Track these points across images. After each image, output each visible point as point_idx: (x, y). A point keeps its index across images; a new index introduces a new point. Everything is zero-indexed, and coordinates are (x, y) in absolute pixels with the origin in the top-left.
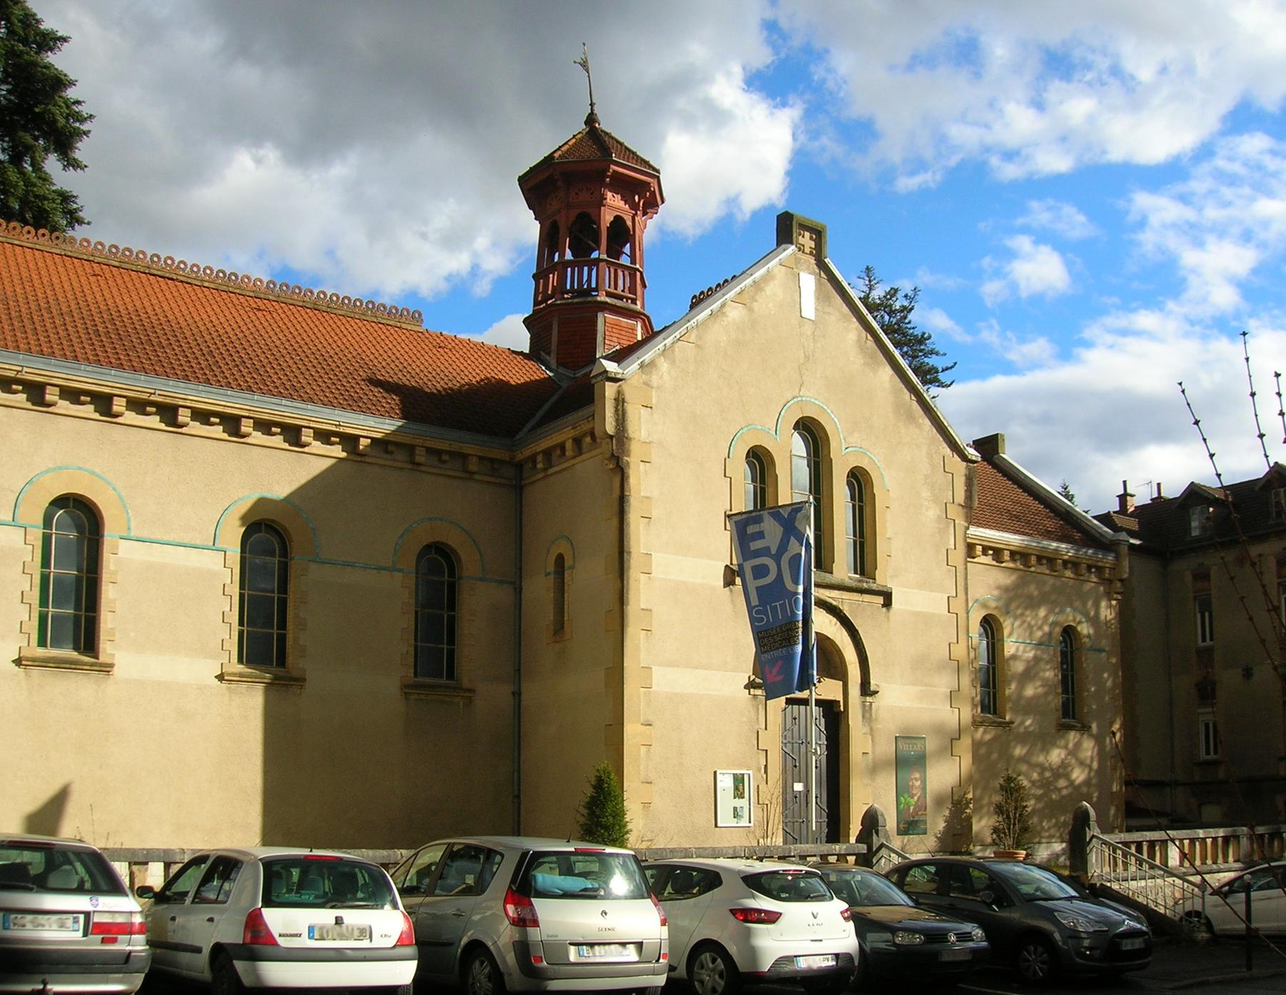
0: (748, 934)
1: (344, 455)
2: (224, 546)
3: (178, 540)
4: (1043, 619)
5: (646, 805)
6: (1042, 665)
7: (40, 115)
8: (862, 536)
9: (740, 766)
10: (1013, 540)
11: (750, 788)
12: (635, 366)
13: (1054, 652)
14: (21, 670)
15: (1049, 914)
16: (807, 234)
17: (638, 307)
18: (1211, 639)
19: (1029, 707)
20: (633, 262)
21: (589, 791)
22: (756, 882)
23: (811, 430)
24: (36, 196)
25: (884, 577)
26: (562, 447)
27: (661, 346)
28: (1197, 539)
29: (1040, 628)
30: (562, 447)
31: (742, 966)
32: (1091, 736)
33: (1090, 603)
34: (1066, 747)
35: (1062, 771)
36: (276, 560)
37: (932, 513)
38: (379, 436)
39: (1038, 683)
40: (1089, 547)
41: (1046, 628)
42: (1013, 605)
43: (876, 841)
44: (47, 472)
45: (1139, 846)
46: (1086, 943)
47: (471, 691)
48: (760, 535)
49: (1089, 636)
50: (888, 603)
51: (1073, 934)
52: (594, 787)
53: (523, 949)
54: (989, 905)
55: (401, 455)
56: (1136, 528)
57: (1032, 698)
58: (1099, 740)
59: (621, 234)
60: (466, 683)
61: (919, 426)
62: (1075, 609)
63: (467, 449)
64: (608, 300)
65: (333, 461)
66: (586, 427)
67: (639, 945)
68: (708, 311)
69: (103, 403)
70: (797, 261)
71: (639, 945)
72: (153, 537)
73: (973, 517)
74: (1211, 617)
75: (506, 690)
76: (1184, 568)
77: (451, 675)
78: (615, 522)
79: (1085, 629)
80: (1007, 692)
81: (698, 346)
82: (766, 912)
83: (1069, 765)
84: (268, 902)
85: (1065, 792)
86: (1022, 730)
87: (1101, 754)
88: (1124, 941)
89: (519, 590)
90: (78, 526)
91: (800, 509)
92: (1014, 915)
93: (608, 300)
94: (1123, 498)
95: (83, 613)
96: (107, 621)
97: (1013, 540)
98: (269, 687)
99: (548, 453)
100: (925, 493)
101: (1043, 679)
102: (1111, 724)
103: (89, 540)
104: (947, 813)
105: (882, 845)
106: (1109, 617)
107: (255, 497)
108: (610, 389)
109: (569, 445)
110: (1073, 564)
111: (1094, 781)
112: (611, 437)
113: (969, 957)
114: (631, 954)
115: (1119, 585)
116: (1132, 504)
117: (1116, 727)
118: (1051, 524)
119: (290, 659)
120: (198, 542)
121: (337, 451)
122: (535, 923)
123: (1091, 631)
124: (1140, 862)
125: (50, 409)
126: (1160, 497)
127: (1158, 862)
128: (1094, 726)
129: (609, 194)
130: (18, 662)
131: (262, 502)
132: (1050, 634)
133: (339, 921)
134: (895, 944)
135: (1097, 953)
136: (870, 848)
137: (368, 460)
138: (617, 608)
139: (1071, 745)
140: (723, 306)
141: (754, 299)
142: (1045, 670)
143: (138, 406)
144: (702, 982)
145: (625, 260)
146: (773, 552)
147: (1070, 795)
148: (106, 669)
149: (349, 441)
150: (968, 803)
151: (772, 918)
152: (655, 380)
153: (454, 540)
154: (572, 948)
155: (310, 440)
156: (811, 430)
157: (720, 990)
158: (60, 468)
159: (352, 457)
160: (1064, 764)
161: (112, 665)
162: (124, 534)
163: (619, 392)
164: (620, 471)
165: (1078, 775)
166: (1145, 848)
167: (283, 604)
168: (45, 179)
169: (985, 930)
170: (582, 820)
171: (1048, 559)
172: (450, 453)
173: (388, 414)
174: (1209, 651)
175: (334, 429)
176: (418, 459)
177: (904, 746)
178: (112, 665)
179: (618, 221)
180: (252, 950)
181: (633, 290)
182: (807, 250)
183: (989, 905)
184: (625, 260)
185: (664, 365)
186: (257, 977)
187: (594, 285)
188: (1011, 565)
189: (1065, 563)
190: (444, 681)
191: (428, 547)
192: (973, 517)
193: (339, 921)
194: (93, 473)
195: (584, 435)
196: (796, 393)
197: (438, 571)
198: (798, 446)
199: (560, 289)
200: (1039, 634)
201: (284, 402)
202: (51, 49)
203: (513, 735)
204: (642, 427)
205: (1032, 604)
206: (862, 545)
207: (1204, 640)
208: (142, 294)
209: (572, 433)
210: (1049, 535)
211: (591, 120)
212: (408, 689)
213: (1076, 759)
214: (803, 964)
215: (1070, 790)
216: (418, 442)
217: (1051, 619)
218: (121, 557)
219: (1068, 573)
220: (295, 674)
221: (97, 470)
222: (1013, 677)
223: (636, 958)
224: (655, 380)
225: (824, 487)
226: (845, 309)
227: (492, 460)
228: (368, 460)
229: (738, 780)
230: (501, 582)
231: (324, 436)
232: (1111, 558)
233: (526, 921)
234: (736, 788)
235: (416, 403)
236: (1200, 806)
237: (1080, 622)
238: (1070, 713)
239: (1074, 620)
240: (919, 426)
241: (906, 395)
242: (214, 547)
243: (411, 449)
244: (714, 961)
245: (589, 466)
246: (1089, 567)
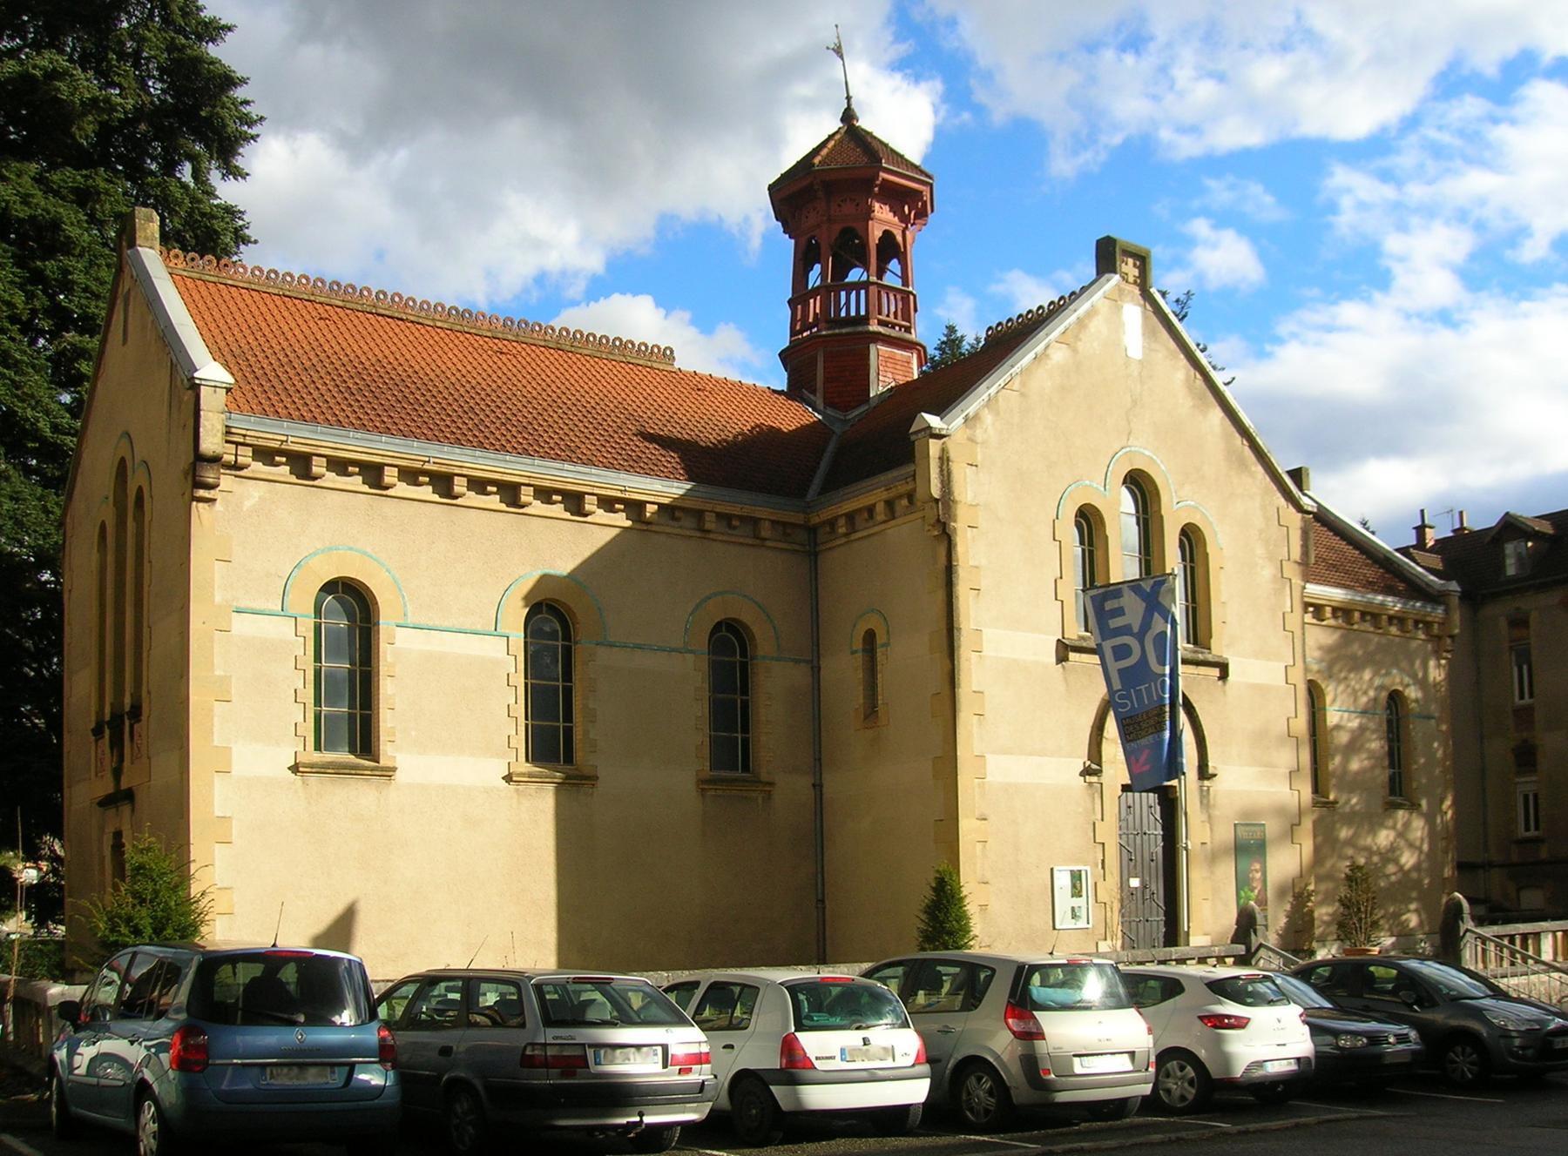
0: (1219, 1040)
1: (628, 523)
2: (507, 632)
3: (457, 626)
4: (1368, 683)
5: (984, 907)
6: (1368, 733)
7: (208, 121)
8: (1194, 601)
9: (1077, 862)
10: (1336, 594)
11: (1087, 885)
12: (960, 420)
13: (1377, 723)
14: (298, 778)
15: (1478, 1013)
16: (1130, 261)
17: (912, 337)
18: (1531, 696)
19: (1352, 783)
20: (905, 282)
21: (930, 894)
22: (1221, 988)
23: (1140, 485)
24: (203, 215)
25: (1220, 647)
26: (870, 510)
27: (985, 397)
28: (1513, 580)
29: (1365, 693)
30: (870, 510)
31: (1215, 1072)
32: (1421, 814)
33: (1418, 663)
34: (1394, 828)
35: (1390, 855)
36: (560, 643)
37: (1267, 572)
38: (666, 501)
39: (1364, 756)
40: (1417, 599)
41: (1372, 693)
42: (1336, 669)
43: (1255, 941)
44: (315, 554)
45: (1512, 939)
46: (1517, 1042)
47: (771, 784)
48: (1120, 612)
49: (1417, 701)
50: (1224, 676)
51: (1505, 1034)
52: (934, 889)
53: (1031, 1063)
54: (1410, 1006)
55: (689, 522)
56: (1440, 567)
57: (1357, 773)
58: (1430, 819)
59: (890, 248)
60: (764, 777)
61: (1252, 475)
62: (1402, 670)
63: (761, 512)
64: (881, 329)
65: (617, 531)
66: (903, 488)
67: (1132, 1054)
68: (1031, 355)
69: (373, 474)
70: (1121, 291)
71: (1132, 1054)
72: (431, 624)
73: (1307, 578)
74: (1530, 670)
75: (804, 783)
76: (1498, 613)
77: (746, 768)
78: (941, 595)
79: (1413, 693)
80: (1331, 767)
81: (1022, 395)
82: (1236, 1017)
83: (1398, 848)
84: (800, 1027)
85: (1393, 878)
86: (1347, 809)
87: (1432, 834)
88: (1557, 1040)
89: (816, 670)
90: (352, 609)
91: (1163, 582)
92: (1438, 1017)
93: (881, 329)
94: (1421, 530)
95: (358, 712)
96: (388, 720)
97: (1336, 594)
98: (560, 788)
99: (850, 517)
100: (1260, 551)
101: (1369, 750)
102: (1442, 801)
103: (361, 628)
104: (1288, 907)
105: (1261, 945)
106: (1439, 679)
107: (535, 575)
108: (934, 447)
109: (880, 507)
110: (1398, 620)
111: (1425, 865)
112: (937, 501)
113: (1407, 1059)
114: (1124, 1064)
115: (1449, 641)
116: (1431, 537)
117: (1448, 802)
118: (1371, 573)
119: (579, 755)
120: (479, 628)
121: (621, 520)
122: (1040, 1035)
123: (1420, 695)
124: (1525, 959)
125: (316, 483)
126: (1462, 528)
127: (1530, 953)
128: (1424, 803)
129: (877, 205)
130: (295, 769)
131: (545, 579)
132: (1375, 699)
133: (866, 1042)
134: (1338, 1048)
135: (1530, 1052)
136: (1248, 949)
137: (654, 528)
138: (947, 691)
139: (1399, 826)
140: (1047, 347)
141: (1077, 338)
142: (1370, 741)
143: (410, 476)
144: (1168, 1091)
145: (891, 280)
146: (1136, 630)
147: (1399, 882)
148: (388, 773)
149: (634, 508)
150: (1310, 895)
151: (1241, 1023)
152: (979, 434)
153: (747, 616)
154: (1076, 1060)
155: (594, 508)
156: (1140, 485)
157: (1190, 1097)
158: (330, 549)
159: (638, 526)
160: (1393, 848)
161: (394, 769)
162: (401, 622)
163: (944, 450)
164: (945, 536)
165: (1408, 859)
166: (1518, 942)
167: (568, 693)
168: (211, 193)
169: (1419, 1031)
170: (922, 926)
171: (1373, 616)
172: (741, 518)
173: (669, 476)
174: (1529, 710)
175: (619, 494)
176: (708, 526)
177: (1242, 832)
178: (394, 769)
179: (888, 236)
180: (792, 1075)
181: (907, 317)
182: (1131, 279)
183: (1410, 1006)
184: (891, 280)
185: (988, 418)
186: (798, 1100)
187: (863, 313)
188: (1332, 622)
189: (1391, 618)
190: (739, 774)
191: (719, 624)
192: (1307, 578)
193: (866, 1042)
194: (365, 553)
195: (900, 497)
196: (1124, 443)
197: (730, 650)
198: (1127, 503)
199: (825, 319)
200: (1364, 700)
201: (566, 466)
202: (213, 40)
203: (815, 834)
204: (970, 489)
205: (1356, 665)
206: (1194, 609)
207: (1522, 697)
208: (279, 317)
209: (885, 495)
210: (1370, 586)
211: (848, 116)
212: (704, 784)
213: (1404, 841)
214: (1273, 1069)
215: (1400, 875)
216: (708, 507)
217: (1377, 682)
218: (398, 647)
219: (1394, 630)
220: (587, 771)
221: (369, 550)
222: (1337, 749)
223: (1130, 1068)
224: (979, 434)
225: (1154, 548)
226: (1172, 344)
227: (784, 524)
228: (654, 528)
229: (1076, 877)
230: (797, 661)
231: (607, 503)
232: (1440, 610)
233: (1032, 1035)
234: (1074, 886)
235: (698, 460)
236: (1519, 890)
237: (1408, 686)
238: (1398, 790)
239: (1401, 683)
240: (1252, 475)
241: (1238, 439)
242: (495, 632)
243: (699, 514)
244: (1182, 1068)
245: (904, 532)
246: (1416, 622)
